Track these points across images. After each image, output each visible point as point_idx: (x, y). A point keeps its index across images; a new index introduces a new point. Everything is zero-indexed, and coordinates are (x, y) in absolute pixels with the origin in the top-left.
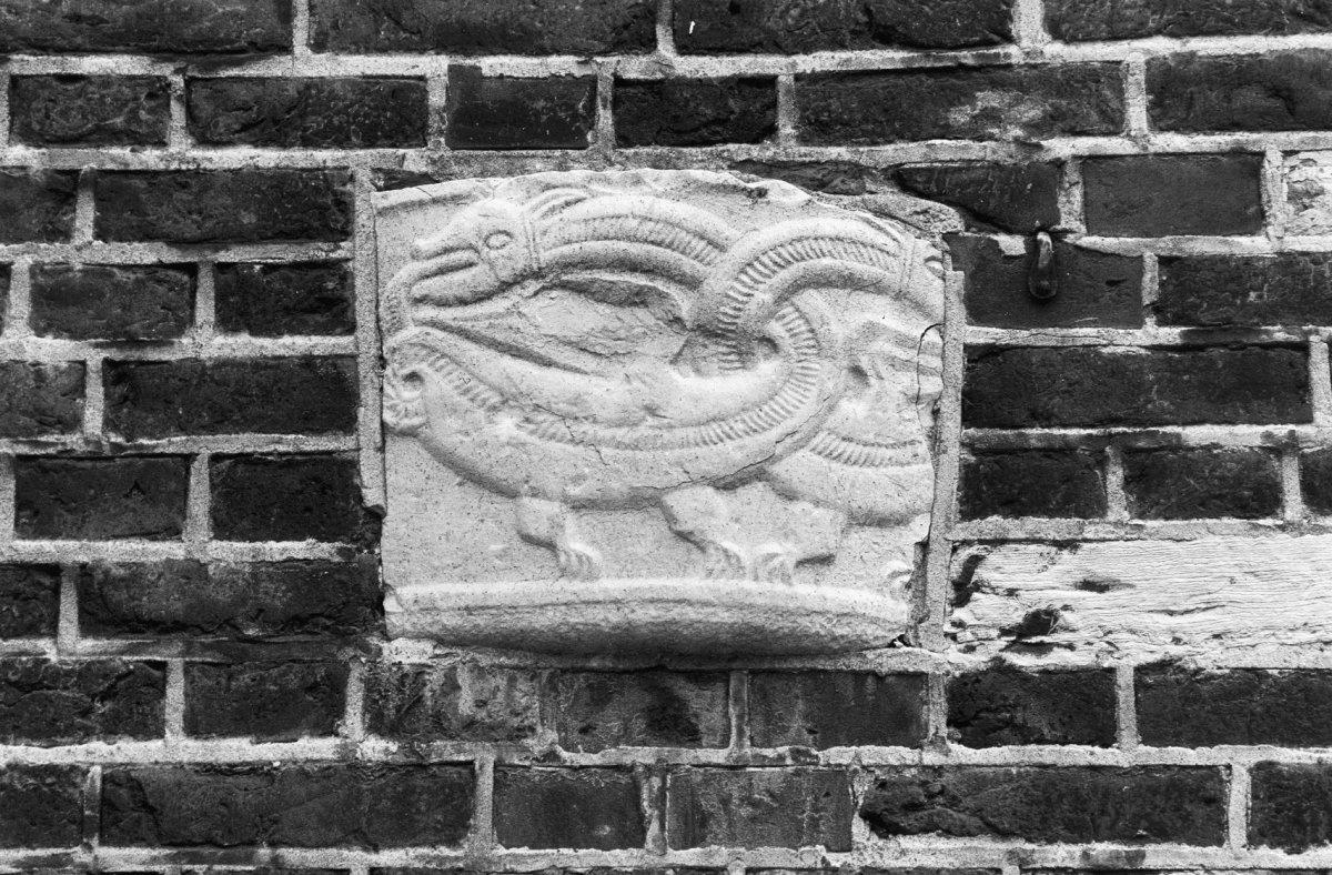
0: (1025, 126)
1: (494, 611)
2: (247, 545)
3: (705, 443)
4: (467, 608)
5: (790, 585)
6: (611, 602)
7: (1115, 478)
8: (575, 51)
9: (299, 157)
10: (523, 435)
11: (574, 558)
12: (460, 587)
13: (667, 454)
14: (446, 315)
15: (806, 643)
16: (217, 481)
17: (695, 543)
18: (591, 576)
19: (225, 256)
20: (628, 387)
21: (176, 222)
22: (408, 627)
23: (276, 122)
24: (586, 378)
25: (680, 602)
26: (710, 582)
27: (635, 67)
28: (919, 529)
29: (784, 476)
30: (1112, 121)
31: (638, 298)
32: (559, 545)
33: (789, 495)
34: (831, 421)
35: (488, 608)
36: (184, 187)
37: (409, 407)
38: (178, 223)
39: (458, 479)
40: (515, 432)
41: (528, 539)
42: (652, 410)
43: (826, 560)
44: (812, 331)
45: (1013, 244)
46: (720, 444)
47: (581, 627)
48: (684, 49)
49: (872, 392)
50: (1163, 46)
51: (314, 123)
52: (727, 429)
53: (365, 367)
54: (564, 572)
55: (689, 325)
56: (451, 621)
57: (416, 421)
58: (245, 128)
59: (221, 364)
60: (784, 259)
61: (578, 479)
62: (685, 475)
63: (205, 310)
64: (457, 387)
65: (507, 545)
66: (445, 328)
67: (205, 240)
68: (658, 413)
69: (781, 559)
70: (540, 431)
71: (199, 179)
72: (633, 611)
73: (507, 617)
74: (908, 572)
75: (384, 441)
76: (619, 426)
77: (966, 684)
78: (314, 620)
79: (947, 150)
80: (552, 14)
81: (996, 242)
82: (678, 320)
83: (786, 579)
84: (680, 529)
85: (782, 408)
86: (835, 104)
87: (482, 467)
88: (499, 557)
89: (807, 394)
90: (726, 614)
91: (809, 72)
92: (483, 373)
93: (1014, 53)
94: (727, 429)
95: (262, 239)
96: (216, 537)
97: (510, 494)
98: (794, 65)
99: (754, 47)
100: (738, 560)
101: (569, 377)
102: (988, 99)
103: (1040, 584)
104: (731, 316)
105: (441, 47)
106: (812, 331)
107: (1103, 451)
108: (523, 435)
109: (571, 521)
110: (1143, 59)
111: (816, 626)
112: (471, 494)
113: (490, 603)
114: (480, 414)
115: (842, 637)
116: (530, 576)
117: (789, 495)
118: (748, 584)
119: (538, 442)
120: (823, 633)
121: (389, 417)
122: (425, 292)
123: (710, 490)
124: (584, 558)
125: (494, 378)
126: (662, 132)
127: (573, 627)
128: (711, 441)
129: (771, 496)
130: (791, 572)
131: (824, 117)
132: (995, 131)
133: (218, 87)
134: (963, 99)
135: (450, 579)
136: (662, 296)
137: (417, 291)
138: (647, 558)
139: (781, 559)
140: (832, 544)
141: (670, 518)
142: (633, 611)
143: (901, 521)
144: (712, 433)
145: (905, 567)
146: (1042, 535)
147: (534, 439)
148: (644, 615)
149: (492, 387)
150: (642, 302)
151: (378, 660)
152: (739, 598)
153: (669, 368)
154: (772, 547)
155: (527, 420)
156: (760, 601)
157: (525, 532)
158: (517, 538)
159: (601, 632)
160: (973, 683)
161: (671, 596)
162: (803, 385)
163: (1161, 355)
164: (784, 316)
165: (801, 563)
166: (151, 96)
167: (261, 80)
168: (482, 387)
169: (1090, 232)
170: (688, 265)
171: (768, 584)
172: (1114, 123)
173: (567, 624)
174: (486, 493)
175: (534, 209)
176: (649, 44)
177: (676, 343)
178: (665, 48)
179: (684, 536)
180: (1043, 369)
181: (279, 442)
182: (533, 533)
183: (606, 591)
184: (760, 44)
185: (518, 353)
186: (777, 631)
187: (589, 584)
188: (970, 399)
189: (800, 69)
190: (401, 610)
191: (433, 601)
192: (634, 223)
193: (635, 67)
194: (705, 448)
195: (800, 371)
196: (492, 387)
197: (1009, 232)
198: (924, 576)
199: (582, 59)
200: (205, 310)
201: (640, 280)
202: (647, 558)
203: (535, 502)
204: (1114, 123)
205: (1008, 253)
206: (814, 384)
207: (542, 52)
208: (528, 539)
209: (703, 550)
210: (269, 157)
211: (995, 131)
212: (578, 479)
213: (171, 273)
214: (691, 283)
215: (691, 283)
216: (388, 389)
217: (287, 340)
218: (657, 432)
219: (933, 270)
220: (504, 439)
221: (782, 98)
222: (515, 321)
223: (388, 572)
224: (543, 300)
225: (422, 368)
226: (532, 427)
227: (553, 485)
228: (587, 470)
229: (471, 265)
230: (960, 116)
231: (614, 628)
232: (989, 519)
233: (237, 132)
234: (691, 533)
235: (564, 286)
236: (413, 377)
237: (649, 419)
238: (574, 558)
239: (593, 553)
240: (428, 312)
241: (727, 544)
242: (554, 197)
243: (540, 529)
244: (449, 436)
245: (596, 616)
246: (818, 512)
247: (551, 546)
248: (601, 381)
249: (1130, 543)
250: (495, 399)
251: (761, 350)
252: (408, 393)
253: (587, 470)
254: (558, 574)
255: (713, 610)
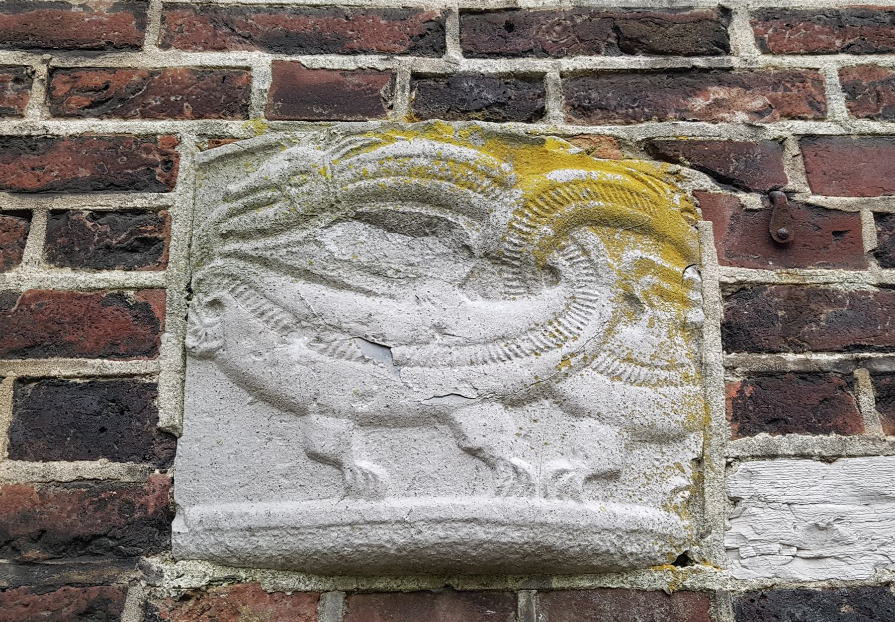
0: (749, 112)
1: (276, 532)
2: (40, 465)
3: (494, 361)
4: (249, 529)
5: (580, 501)
6: (397, 522)
7: (867, 399)
8: (380, 52)
9: (138, 126)
10: (314, 354)
11: (360, 476)
12: (244, 507)
13: (456, 371)
14: (246, 247)
15: (596, 562)
16: (19, 402)
17: (484, 460)
18: (377, 495)
19: (59, 203)
20: (418, 307)
21: (19, 176)
22: (192, 548)
23: (122, 100)
24: (378, 300)
25: (468, 521)
26: (498, 500)
27: (427, 64)
28: (693, 446)
29: (570, 393)
30: (819, 110)
31: (427, 228)
32: (344, 459)
33: (576, 412)
34: (613, 344)
35: (270, 528)
36: (34, 150)
37: (209, 331)
38: (22, 177)
39: (250, 399)
40: (306, 351)
41: (315, 457)
42: (440, 329)
43: (612, 476)
44: (590, 261)
45: (753, 200)
46: (508, 362)
47: (365, 549)
48: (467, 54)
49: (646, 317)
50: (847, 59)
51: (154, 102)
52: (514, 347)
53: (176, 293)
54: (349, 491)
55: (477, 253)
56: (237, 542)
57: (214, 344)
58: (94, 105)
59: (38, 295)
60: (564, 198)
61: (363, 396)
62: (473, 391)
63: (35, 246)
64: (253, 311)
65: (294, 463)
66: (243, 257)
67: (44, 190)
68: (447, 331)
69: (570, 475)
70: (330, 350)
71: (51, 141)
72: (420, 532)
73: (291, 539)
74: (687, 488)
75: (185, 366)
76: (409, 344)
77: (752, 601)
78: (97, 542)
79: (687, 130)
80: (361, 25)
81: (738, 198)
82: (468, 248)
83: (576, 496)
84: (469, 445)
85: (566, 328)
86: (594, 95)
87: (272, 386)
88: (285, 476)
89: (588, 317)
90: (517, 534)
91: (571, 69)
92: (280, 296)
93: (735, 61)
94: (514, 347)
95: (94, 190)
96: (9, 457)
97: (296, 410)
98: (560, 64)
99: (525, 52)
100: (528, 477)
101: (361, 299)
102: (719, 93)
103: (813, 498)
104: (515, 245)
105: (269, 44)
106: (590, 261)
107: (852, 374)
108: (314, 354)
109: (358, 438)
110: (836, 67)
111: (605, 543)
112: (263, 414)
113: (273, 524)
114: (273, 336)
115: (631, 554)
116: (315, 495)
117: (576, 412)
118: (538, 501)
119: (328, 360)
120: (612, 550)
121: (190, 342)
122: (232, 228)
123: (498, 406)
124: (370, 476)
125: (289, 301)
126: (451, 112)
127: (357, 549)
128: (500, 358)
129: (558, 413)
130: (580, 488)
131: (586, 103)
132: (726, 115)
133: (77, 74)
134: (697, 92)
135: (236, 498)
136: (450, 226)
137: (224, 227)
138: (435, 475)
139: (570, 475)
140: (618, 461)
141: (459, 435)
142: (420, 532)
143: (679, 438)
144: (500, 352)
145: (684, 482)
146: (809, 450)
147: (324, 358)
148: (431, 535)
149: (285, 309)
150: (433, 233)
151: (158, 584)
152: (529, 517)
153: (458, 291)
154: (561, 463)
155: (319, 340)
156: (550, 519)
157: (312, 449)
158: (304, 455)
159: (386, 555)
160: (759, 599)
161: (459, 515)
162: (584, 308)
163: (885, 292)
164: (564, 247)
165: (589, 479)
166: (17, 80)
167: (113, 70)
168: (277, 310)
169: (813, 193)
170: (476, 198)
171: (557, 501)
172: (820, 112)
173: (351, 545)
174: (275, 411)
175: (333, 153)
176: (440, 50)
177: (463, 269)
178: (454, 52)
179: (473, 452)
180: (791, 302)
181: (85, 365)
182: (319, 451)
183: (393, 510)
184: (531, 51)
185: (308, 275)
186: (567, 550)
187: (375, 504)
188: (728, 328)
189: (564, 69)
190: (187, 530)
191: (217, 521)
192: (425, 162)
193: (427, 64)
194: (493, 366)
195: (581, 296)
196: (285, 309)
197: (747, 190)
198: (702, 493)
199: (385, 57)
200: (35, 246)
201: (433, 212)
202: (435, 475)
203: (323, 418)
204: (820, 112)
205: (749, 207)
206: (594, 308)
207: (354, 52)
208: (315, 457)
209: (493, 467)
210: (111, 126)
211: (726, 115)
212: (363, 396)
213: (8, 218)
214: (479, 215)
215: (479, 215)
216: (192, 317)
217: (105, 274)
218: (446, 349)
219: (688, 220)
220: (295, 358)
221: (550, 89)
222: (312, 248)
223: (179, 495)
224: (339, 229)
225: (224, 294)
226: (323, 346)
227: (341, 402)
228: (375, 388)
229: (275, 201)
230: (699, 103)
231: (399, 550)
232: (757, 437)
233: (87, 107)
234: (480, 450)
235: (359, 217)
236: (216, 304)
237: (437, 336)
238: (360, 476)
239: (378, 470)
240: (232, 246)
241: (516, 461)
242: (351, 142)
243: (326, 447)
244: (243, 356)
245: (381, 536)
246: (603, 429)
247: (337, 464)
248: (391, 302)
249: (889, 458)
250: (287, 319)
251: (544, 276)
252: (209, 318)
253: (375, 388)
254: (342, 492)
255: (503, 529)
